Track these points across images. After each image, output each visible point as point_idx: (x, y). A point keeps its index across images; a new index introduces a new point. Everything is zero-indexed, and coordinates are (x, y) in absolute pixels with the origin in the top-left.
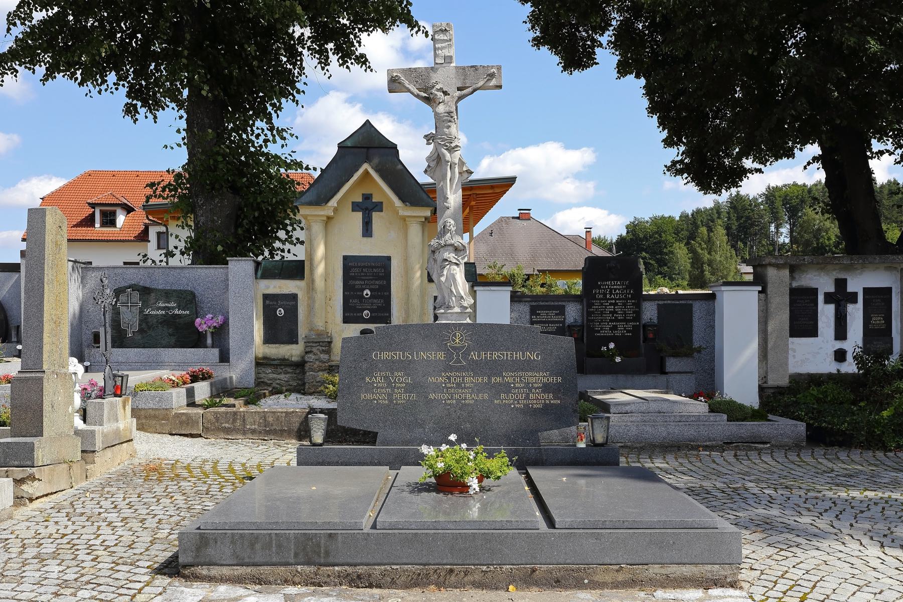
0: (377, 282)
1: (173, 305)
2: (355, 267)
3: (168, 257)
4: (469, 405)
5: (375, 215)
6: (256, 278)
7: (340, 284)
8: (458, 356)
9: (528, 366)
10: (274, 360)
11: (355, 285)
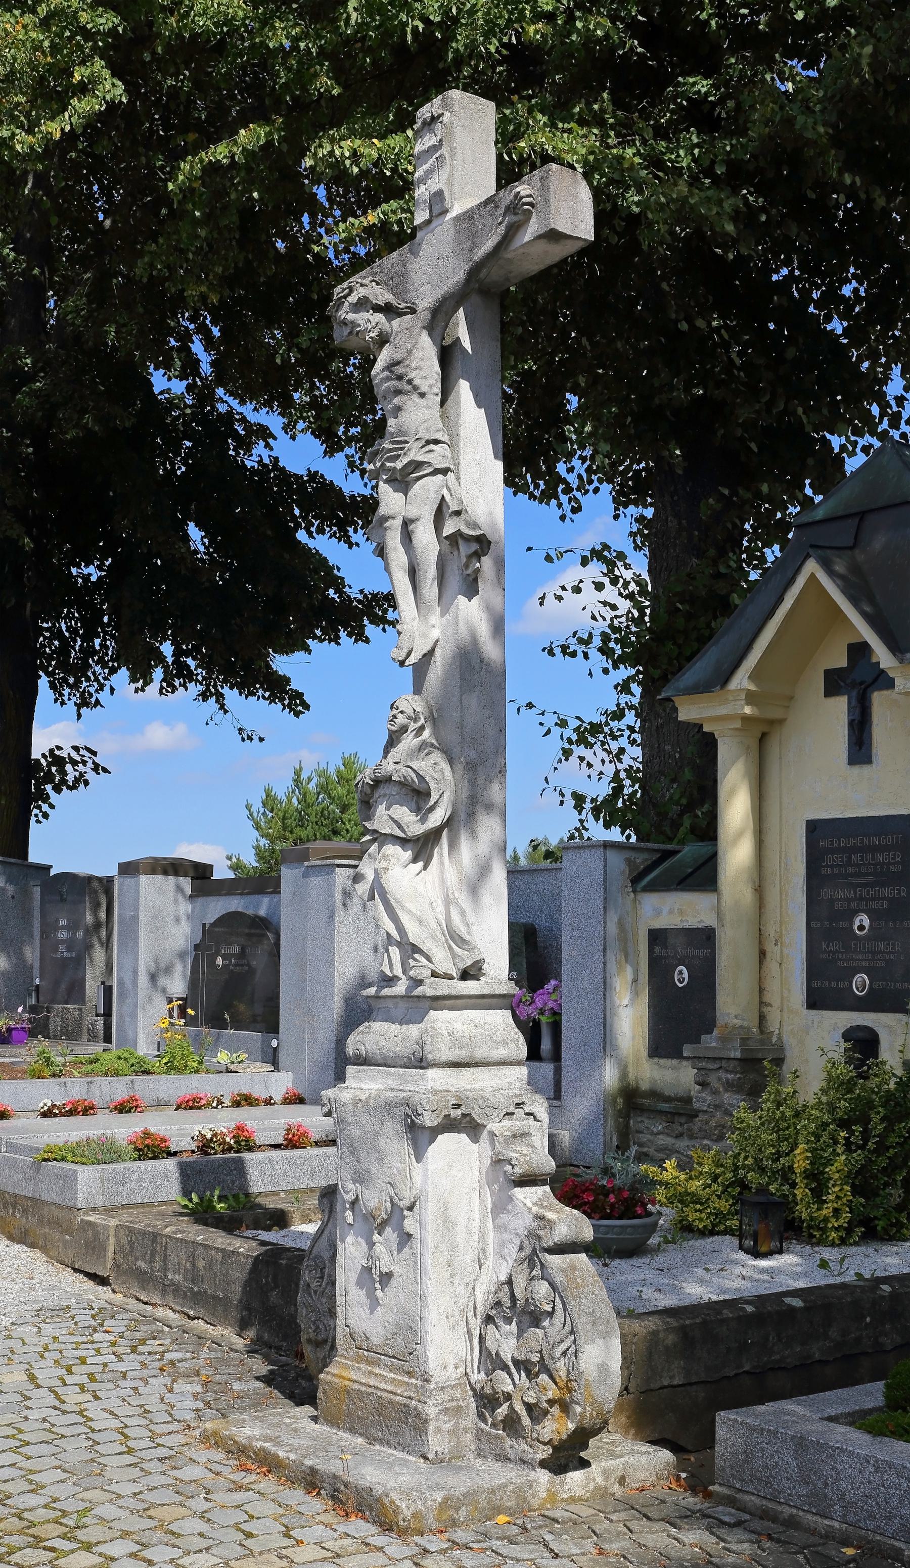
0: (886, 892)
2: (832, 851)
3: (543, 848)
5: (878, 699)
7: (801, 899)
10: (668, 1099)
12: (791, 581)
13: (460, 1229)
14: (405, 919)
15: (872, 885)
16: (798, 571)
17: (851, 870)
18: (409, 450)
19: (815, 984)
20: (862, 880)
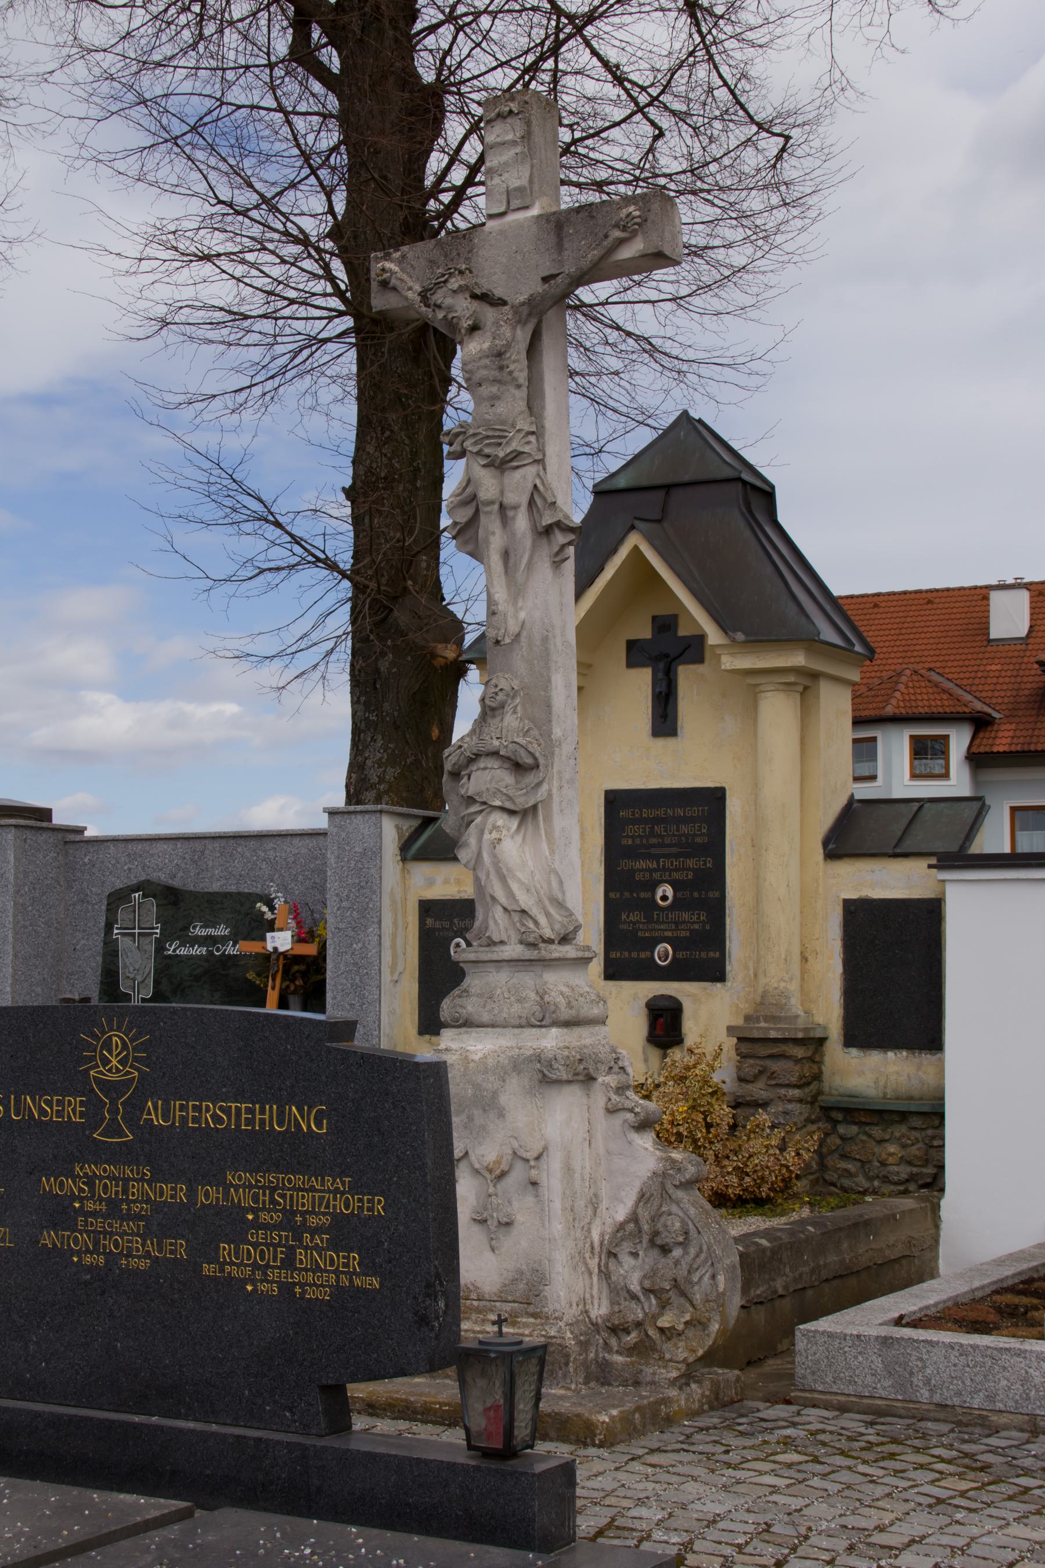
0: (690, 863)
1: (222, 931)
2: (634, 822)
4: (136, 1272)
6: (404, 860)
8: (114, 1111)
9: (289, 1153)
11: (632, 872)
12: (614, 551)
13: (577, 1176)
14: (514, 887)
15: (676, 856)
16: (621, 541)
17: (653, 841)
18: (511, 439)
19: (613, 955)
20: (666, 851)
